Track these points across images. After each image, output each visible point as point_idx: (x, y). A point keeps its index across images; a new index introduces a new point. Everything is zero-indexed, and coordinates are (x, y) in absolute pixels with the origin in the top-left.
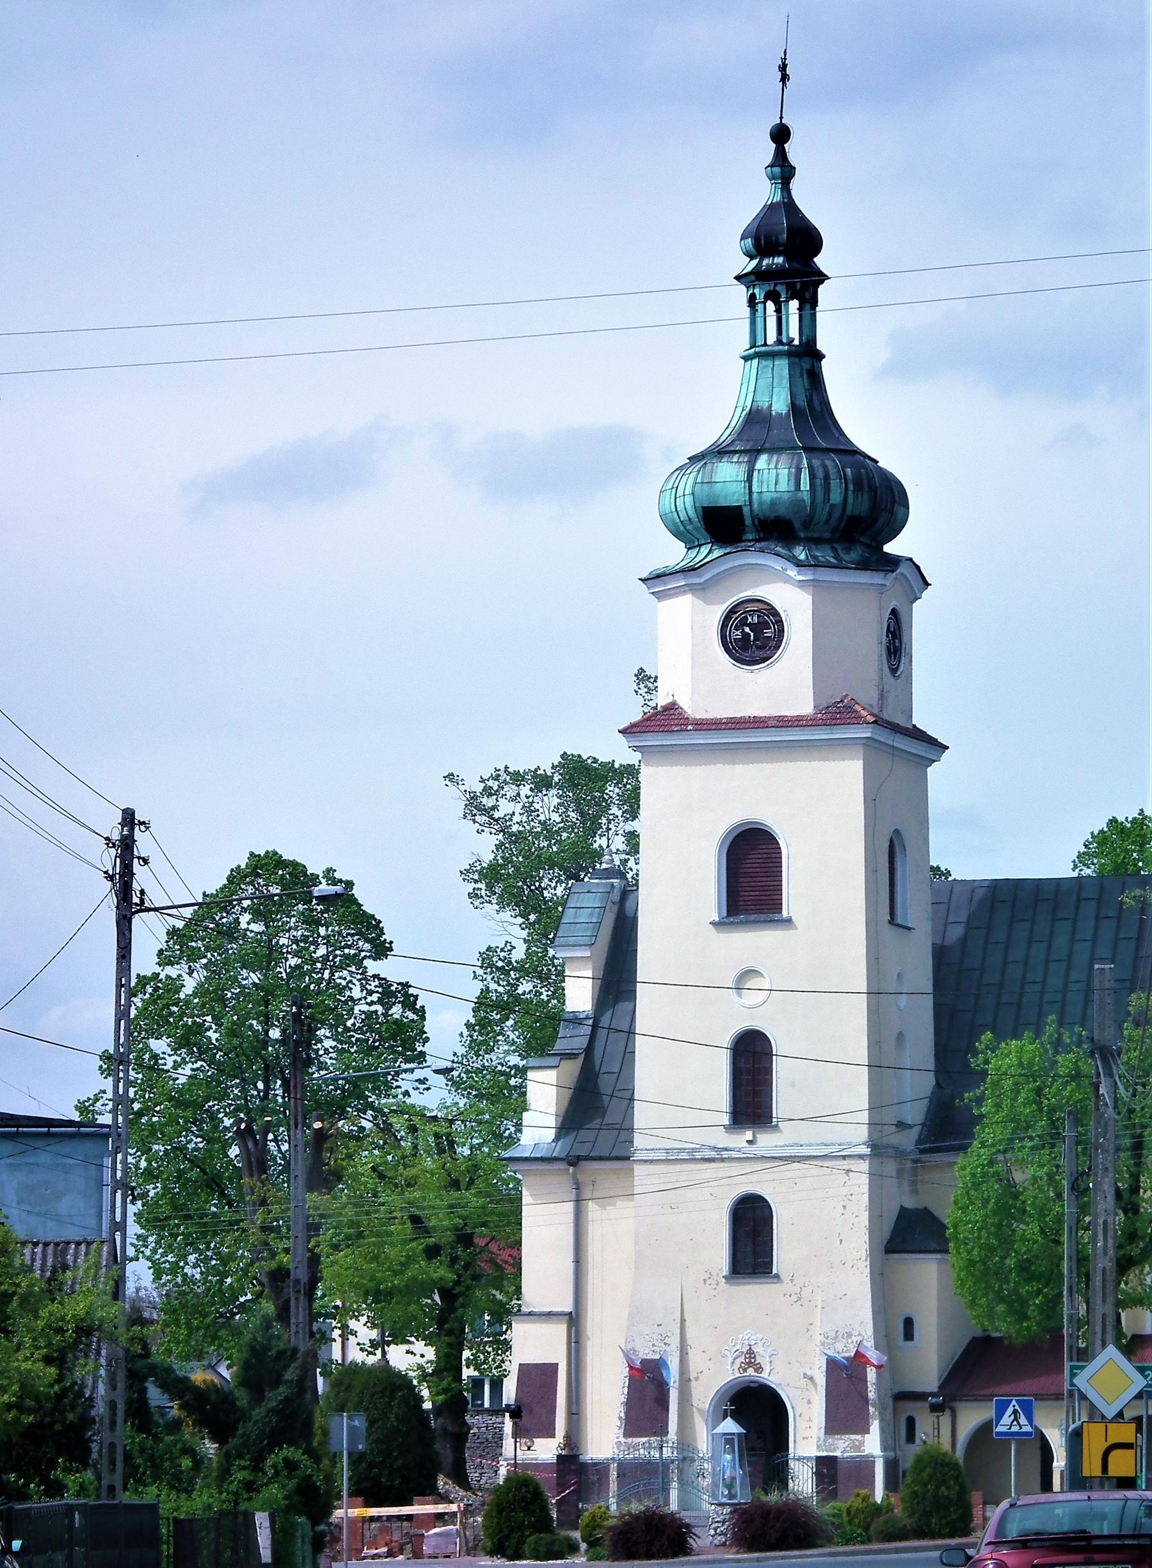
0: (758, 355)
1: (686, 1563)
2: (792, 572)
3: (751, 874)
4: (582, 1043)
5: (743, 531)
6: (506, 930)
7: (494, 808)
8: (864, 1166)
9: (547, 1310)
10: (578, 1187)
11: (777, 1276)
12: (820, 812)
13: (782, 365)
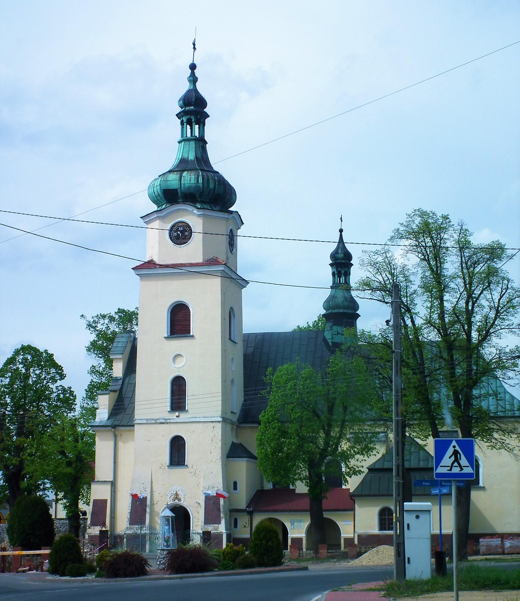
0: (184, 140)
1: (144, 580)
2: (196, 211)
3: (179, 321)
4: (118, 387)
5: (178, 199)
6: (100, 363)
7: (96, 326)
8: (220, 425)
9: (104, 480)
10: (115, 436)
11: (187, 466)
12: (204, 298)
13: (193, 143)
